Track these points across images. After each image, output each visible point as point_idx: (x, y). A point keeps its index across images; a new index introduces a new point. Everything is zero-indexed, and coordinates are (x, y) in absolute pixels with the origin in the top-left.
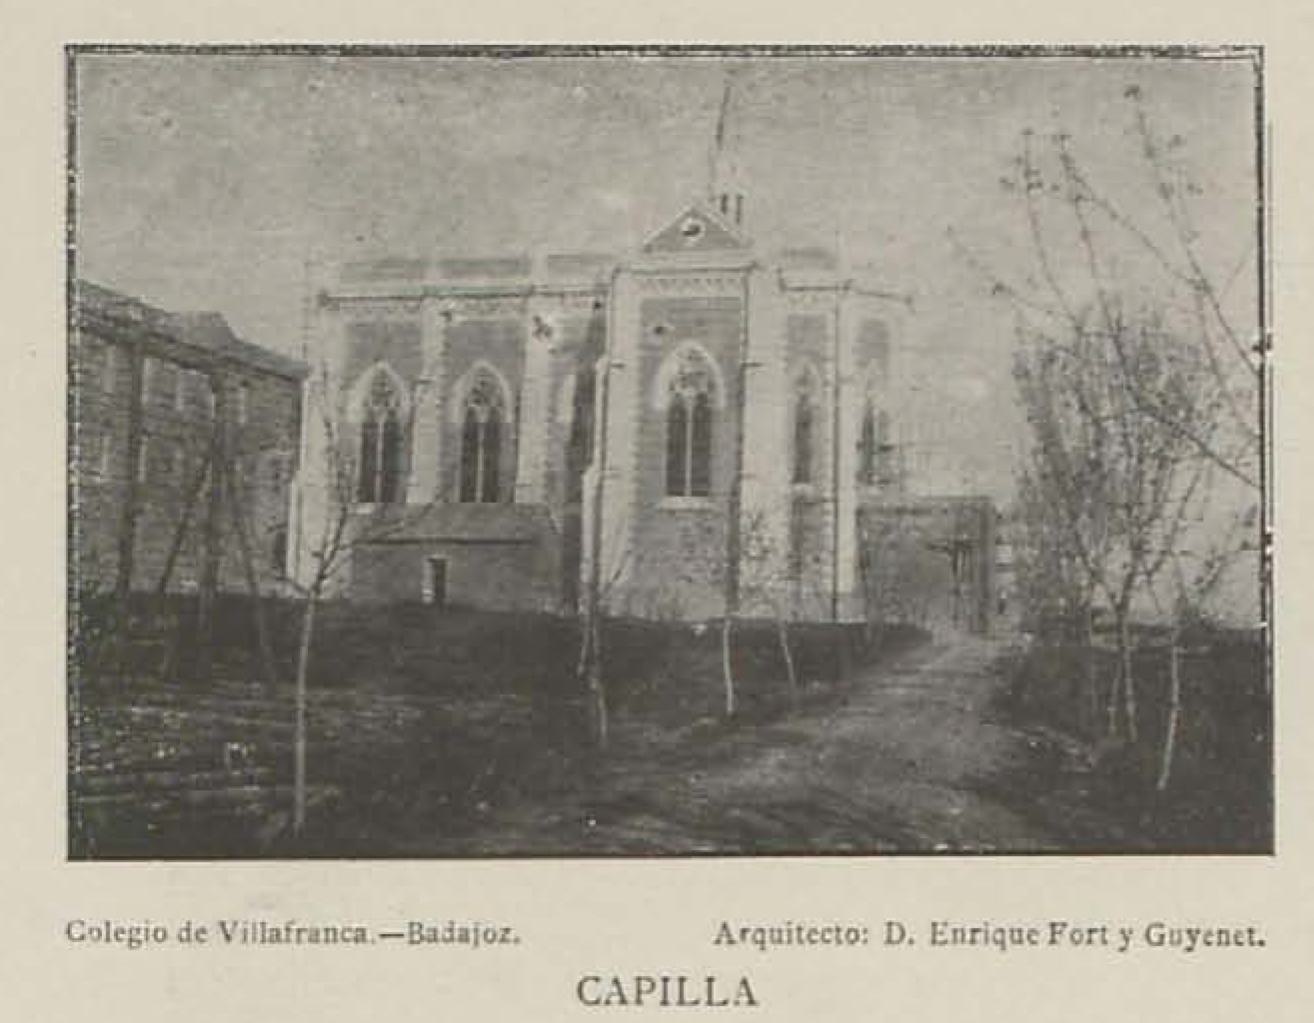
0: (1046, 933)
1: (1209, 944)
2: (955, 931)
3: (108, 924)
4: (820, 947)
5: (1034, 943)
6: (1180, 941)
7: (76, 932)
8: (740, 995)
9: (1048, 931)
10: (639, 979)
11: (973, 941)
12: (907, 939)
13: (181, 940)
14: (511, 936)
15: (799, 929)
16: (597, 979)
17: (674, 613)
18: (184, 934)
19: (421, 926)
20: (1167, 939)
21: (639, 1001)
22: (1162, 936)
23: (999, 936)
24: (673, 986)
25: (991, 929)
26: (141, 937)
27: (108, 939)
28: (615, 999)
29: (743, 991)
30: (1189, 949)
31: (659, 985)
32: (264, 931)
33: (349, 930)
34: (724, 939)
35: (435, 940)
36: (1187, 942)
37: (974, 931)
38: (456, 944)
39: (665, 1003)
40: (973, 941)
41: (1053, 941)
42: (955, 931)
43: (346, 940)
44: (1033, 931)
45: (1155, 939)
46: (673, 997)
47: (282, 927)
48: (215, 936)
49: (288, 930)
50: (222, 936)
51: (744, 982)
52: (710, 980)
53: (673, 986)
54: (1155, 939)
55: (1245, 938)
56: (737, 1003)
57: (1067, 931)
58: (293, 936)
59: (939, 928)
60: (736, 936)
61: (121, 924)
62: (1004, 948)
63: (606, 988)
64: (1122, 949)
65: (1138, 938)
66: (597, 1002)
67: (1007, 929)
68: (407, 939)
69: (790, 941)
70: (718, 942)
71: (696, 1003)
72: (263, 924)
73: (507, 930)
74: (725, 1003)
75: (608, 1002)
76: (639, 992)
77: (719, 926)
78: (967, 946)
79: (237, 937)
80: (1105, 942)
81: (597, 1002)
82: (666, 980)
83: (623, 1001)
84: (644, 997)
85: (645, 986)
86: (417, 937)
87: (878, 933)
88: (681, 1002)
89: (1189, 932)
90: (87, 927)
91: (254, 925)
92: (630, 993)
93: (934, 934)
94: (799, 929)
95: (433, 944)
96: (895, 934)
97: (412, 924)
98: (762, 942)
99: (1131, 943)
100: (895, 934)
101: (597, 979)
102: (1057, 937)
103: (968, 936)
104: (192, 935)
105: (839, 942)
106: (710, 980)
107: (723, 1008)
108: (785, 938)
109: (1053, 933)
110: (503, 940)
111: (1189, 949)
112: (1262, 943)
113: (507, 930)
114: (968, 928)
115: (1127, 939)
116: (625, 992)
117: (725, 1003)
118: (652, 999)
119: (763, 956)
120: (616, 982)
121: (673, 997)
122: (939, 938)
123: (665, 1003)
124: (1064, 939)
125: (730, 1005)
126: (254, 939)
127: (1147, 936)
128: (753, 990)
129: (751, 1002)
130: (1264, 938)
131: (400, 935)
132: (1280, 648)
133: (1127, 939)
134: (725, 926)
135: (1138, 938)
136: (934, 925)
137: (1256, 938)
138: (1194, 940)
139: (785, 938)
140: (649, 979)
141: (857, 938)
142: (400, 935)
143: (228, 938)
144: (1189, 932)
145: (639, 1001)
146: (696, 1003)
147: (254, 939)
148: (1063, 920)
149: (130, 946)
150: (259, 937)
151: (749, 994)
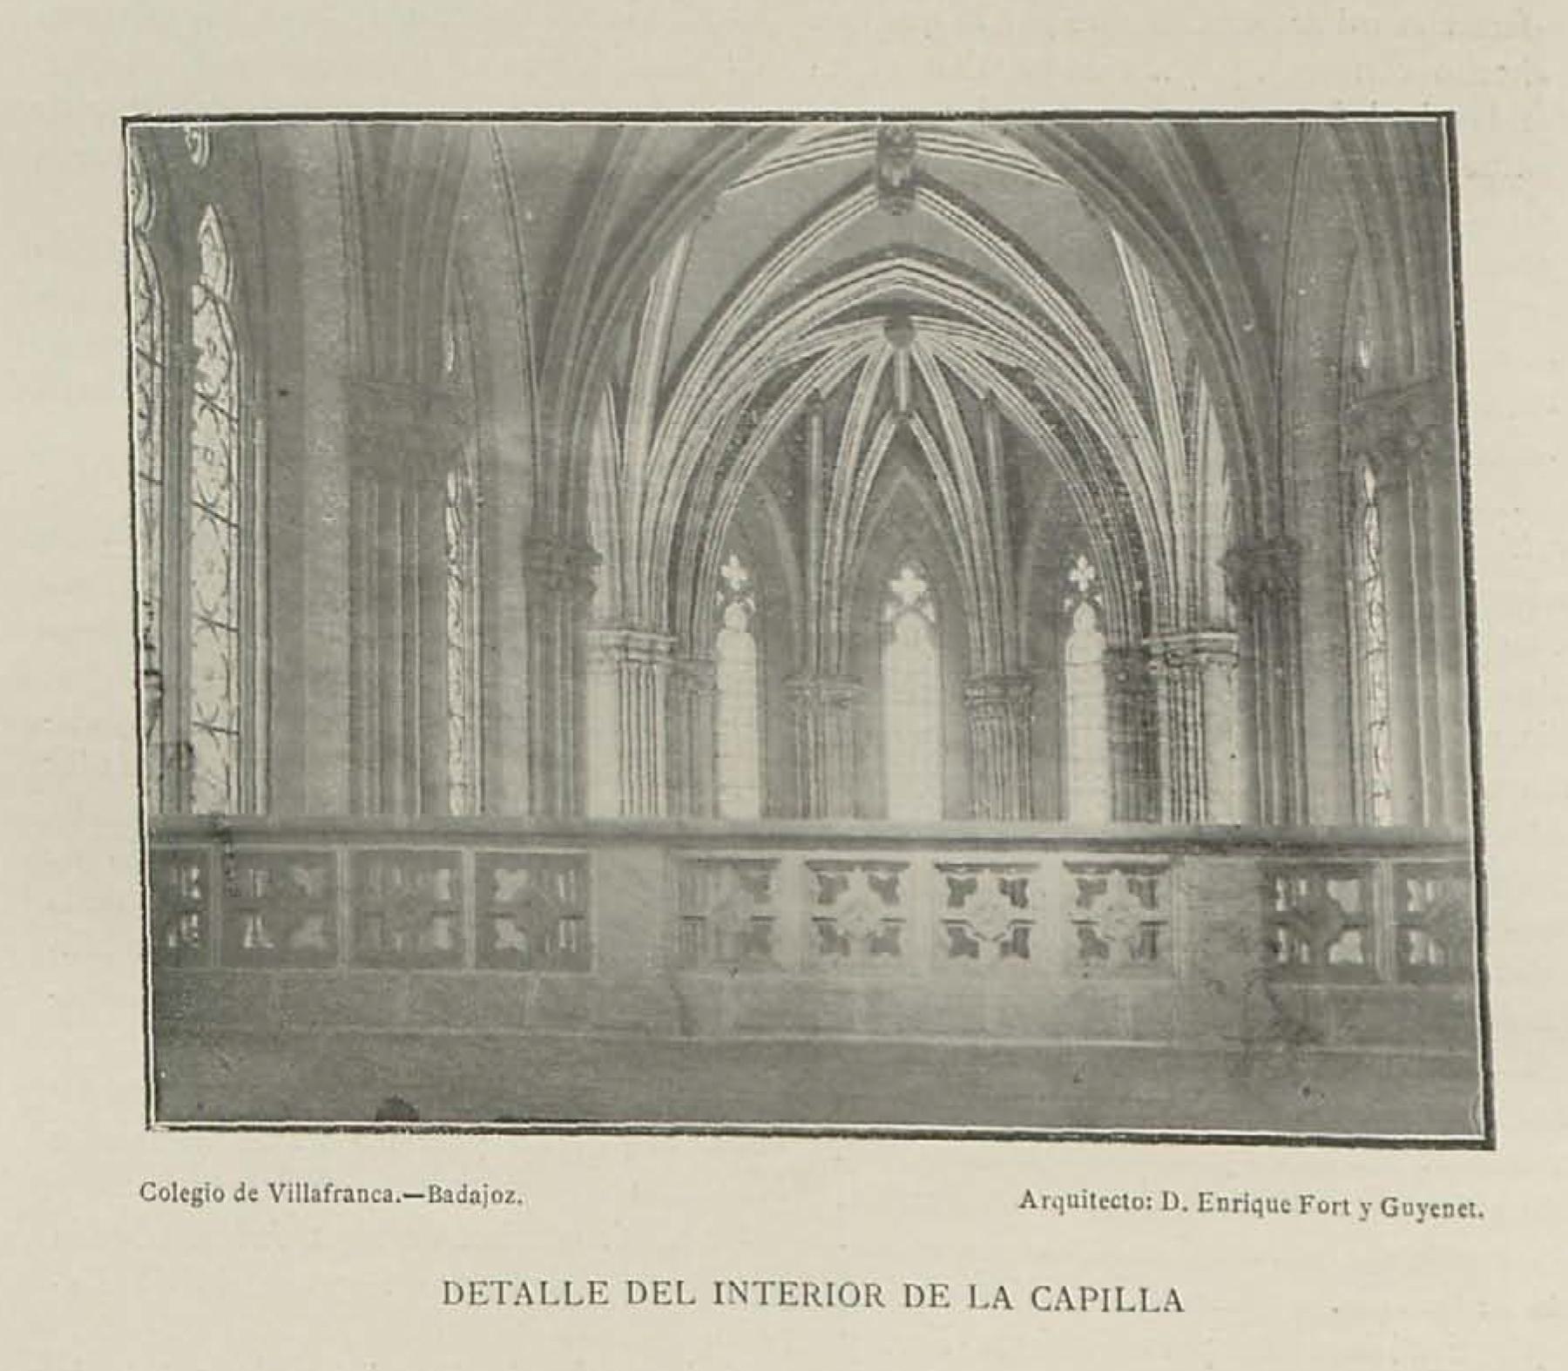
0: (1296, 1205)
1: (1435, 1215)
2: (1220, 1200)
5: (1286, 1211)
6: (1412, 1213)
7: (149, 1192)
9: (1299, 1201)
11: (1236, 1210)
13: (238, 1199)
14: (516, 1197)
15: (1093, 1196)
16: (1048, 1289)
20: (1400, 1211)
21: (1084, 1308)
22: (1395, 1208)
23: (1257, 1206)
25: (1250, 1199)
26: (203, 1197)
27: (175, 1199)
28: (1064, 1305)
30: (1420, 1221)
31: (1101, 1294)
36: (1418, 1215)
37: (1236, 1201)
39: (1106, 1309)
40: (1236, 1210)
41: (1303, 1212)
42: (1220, 1200)
44: (1286, 1202)
45: (1389, 1210)
46: (1112, 1304)
47: (322, 1188)
48: (264, 1193)
49: (327, 1191)
53: (1112, 1295)
54: (1389, 1210)
56: (1057, 1308)
58: (331, 1196)
59: (1206, 1197)
60: (1039, 1203)
61: (1106, 1194)
64: (1363, 1219)
65: (1375, 1210)
66: (1048, 1308)
68: (427, 1198)
70: (1023, 1206)
71: (1133, 1309)
74: (1157, 1310)
75: (1057, 1308)
78: (1230, 1214)
79: (284, 1197)
80: (1347, 1213)
81: (1048, 1308)
82: (1106, 1291)
83: (1070, 1307)
84: (1088, 1304)
87: (1157, 1202)
88: (1120, 1308)
89: (1419, 1205)
90: (158, 1187)
94: (1093, 1196)
96: (1170, 1201)
97: (431, 1188)
98: (1261, 1211)
99: (1371, 1213)
101: (1048, 1289)
103: (1231, 1206)
104: (245, 1195)
105: (1126, 1207)
108: (1081, 1202)
109: (1304, 1204)
111: (1420, 1221)
114: (1231, 1198)
115: (1366, 1211)
117: (1157, 1310)
118: (1095, 1307)
119: (1261, 1221)
120: (1064, 1291)
121: (1112, 1304)
122: (1206, 1206)
123: (1106, 1309)
127: (1383, 1208)
130: (1483, 1210)
131: (421, 1196)
133: (1366, 1211)
134: (1029, 1193)
135: (1375, 1210)
138: (1423, 1212)
139: (1081, 1202)
142: (421, 1196)
143: (277, 1199)
144: (1419, 1205)
150: (302, 1196)
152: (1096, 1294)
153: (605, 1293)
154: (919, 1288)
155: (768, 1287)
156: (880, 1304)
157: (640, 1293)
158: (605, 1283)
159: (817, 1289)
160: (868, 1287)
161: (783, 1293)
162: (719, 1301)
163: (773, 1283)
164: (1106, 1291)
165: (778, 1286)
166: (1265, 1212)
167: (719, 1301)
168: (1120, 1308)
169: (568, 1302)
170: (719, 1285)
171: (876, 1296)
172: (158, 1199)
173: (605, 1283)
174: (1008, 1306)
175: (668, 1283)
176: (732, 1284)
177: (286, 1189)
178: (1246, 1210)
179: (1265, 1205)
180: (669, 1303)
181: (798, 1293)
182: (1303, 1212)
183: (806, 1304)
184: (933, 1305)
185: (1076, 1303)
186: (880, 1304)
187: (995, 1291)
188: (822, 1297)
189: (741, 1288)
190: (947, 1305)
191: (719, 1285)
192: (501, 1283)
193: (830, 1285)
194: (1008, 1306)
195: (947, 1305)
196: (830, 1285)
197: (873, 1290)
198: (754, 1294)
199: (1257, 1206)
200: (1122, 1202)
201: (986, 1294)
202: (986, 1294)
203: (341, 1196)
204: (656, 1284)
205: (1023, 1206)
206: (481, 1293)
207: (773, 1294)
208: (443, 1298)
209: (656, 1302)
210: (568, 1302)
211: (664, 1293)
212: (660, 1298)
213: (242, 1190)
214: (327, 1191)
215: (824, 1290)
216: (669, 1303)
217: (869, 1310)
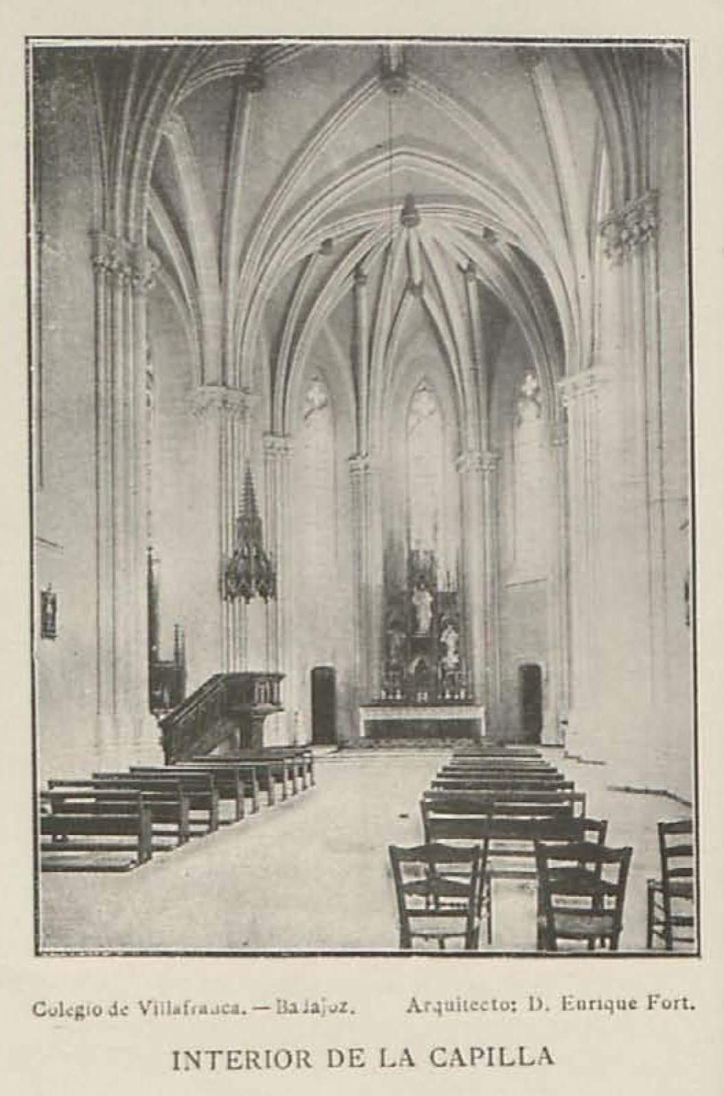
3: (61, 1004)
4: (479, 1013)
5: (124, 1014)
7: (40, 1010)
8: (403, 1060)
10: (472, 1049)
12: (544, 1007)
13: (111, 1014)
16: (443, 1049)
17: (647, 828)
18: (113, 1011)
19: (285, 1002)
21: (473, 1063)
24: (496, 1053)
29: (406, 1057)
31: (487, 1052)
32: (169, 1007)
33: (228, 1006)
34: (414, 1009)
35: (295, 1011)
38: (309, 1014)
39: (491, 1064)
41: (650, 1008)
43: (225, 1013)
46: (496, 1060)
48: (135, 1011)
49: (186, 1006)
50: (141, 1011)
51: (406, 1051)
52: (522, 1049)
53: (496, 1053)
55: (680, 1004)
56: (401, 1065)
57: (660, 1000)
62: (612, 1012)
63: (449, 1056)
66: (444, 1065)
67: (615, 1001)
69: (459, 1010)
70: (409, 1011)
71: (512, 1064)
72: (169, 1003)
73: (345, 1004)
74: (393, 1065)
75: (452, 1065)
76: (473, 1058)
77: (410, 1000)
79: (151, 1011)
81: (444, 1065)
82: (490, 1049)
83: (462, 1064)
84: (476, 1061)
85: (477, 1053)
86: (282, 1010)
91: (162, 1003)
92: (466, 1059)
93: (564, 1003)
95: (294, 1015)
96: (535, 1004)
98: (612, 1008)
100: (535, 1004)
101: (443, 1049)
102: (653, 1005)
103: (588, 1005)
105: (495, 1009)
106: (522, 1049)
107: (361, 1069)
108: (456, 1007)
109: (650, 1003)
110: (342, 1011)
112: (693, 1008)
113: (345, 1004)
116: (463, 1057)
120: (457, 1051)
121: (496, 1060)
123: (491, 1064)
124: (657, 1006)
125: (536, 1065)
126: (162, 1013)
128: (413, 1057)
129: (412, 1064)
132: (138, 632)
136: (564, 998)
137: (689, 1004)
139: (456, 1007)
140: (479, 1049)
141: (508, 1007)
143: (145, 1012)
145: (473, 1063)
146: (512, 1064)
147: (162, 1013)
148: (657, 992)
149: (77, 1019)
151: (409, 1059)
152: (482, 1053)
153: (362, 1056)
154: (340, 1053)
155: (217, 1055)
156: (308, 1065)
157: (279, 1059)
158: (361, 1050)
159: (257, 1055)
160: (298, 1052)
161: (230, 1060)
162: (176, 1068)
163: (220, 1052)
164: (490, 1049)
165: (225, 1056)
166: (616, 1010)
167: (176, 1068)
168: (502, 1064)
169: (522, 1063)
170: (176, 1053)
171: (305, 1060)
172: (47, 1015)
173: (361, 1050)
174: (550, 1062)
175: (239, 1052)
176: (188, 1053)
177: (152, 1006)
178: (600, 1008)
179: (615, 1004)
180: (240, 1068)
181: (242, 1060)
182: (650, 1008)
183: (248, 1067)
184: (352, 1065)
185: (467, 1060)
186: (308, 1065)
187: (540, 1050)
188: (261, 1061)
189: (195, 1057)
190: (362, 1065)
191: (176, 1053)
192: (213, 1053)
193: (268, 1052)
194: (550, 1062)
195: (362, 1065)
196: (268, 1052)
197: (303, 1055)
198: (205, 1060)
199: (609, 1004)
200: (490, 1005)
201: (393, 1055)
202: (393, 1055)
203: (197, 1010)
204: (351, 1051)
205: (409, 1011)
206: (236, 1060)
207: (221, 1060)
208: (327, 1062)
209: (352, 1065)
210: (522, 1063)
211: (236, 1060)
212: (356, 1062)
213: (115, 1007)
214: (186, 1006)
215: (263, 1055)
216: (240, 1068)
217: (298, 1071)
